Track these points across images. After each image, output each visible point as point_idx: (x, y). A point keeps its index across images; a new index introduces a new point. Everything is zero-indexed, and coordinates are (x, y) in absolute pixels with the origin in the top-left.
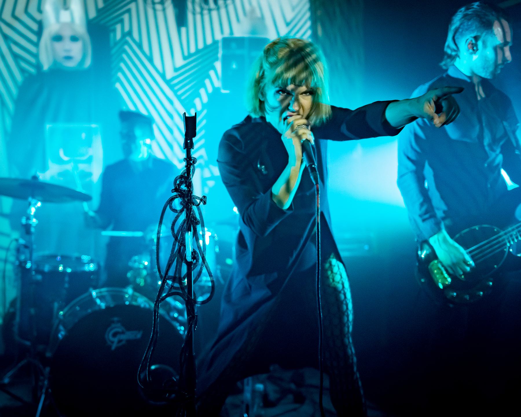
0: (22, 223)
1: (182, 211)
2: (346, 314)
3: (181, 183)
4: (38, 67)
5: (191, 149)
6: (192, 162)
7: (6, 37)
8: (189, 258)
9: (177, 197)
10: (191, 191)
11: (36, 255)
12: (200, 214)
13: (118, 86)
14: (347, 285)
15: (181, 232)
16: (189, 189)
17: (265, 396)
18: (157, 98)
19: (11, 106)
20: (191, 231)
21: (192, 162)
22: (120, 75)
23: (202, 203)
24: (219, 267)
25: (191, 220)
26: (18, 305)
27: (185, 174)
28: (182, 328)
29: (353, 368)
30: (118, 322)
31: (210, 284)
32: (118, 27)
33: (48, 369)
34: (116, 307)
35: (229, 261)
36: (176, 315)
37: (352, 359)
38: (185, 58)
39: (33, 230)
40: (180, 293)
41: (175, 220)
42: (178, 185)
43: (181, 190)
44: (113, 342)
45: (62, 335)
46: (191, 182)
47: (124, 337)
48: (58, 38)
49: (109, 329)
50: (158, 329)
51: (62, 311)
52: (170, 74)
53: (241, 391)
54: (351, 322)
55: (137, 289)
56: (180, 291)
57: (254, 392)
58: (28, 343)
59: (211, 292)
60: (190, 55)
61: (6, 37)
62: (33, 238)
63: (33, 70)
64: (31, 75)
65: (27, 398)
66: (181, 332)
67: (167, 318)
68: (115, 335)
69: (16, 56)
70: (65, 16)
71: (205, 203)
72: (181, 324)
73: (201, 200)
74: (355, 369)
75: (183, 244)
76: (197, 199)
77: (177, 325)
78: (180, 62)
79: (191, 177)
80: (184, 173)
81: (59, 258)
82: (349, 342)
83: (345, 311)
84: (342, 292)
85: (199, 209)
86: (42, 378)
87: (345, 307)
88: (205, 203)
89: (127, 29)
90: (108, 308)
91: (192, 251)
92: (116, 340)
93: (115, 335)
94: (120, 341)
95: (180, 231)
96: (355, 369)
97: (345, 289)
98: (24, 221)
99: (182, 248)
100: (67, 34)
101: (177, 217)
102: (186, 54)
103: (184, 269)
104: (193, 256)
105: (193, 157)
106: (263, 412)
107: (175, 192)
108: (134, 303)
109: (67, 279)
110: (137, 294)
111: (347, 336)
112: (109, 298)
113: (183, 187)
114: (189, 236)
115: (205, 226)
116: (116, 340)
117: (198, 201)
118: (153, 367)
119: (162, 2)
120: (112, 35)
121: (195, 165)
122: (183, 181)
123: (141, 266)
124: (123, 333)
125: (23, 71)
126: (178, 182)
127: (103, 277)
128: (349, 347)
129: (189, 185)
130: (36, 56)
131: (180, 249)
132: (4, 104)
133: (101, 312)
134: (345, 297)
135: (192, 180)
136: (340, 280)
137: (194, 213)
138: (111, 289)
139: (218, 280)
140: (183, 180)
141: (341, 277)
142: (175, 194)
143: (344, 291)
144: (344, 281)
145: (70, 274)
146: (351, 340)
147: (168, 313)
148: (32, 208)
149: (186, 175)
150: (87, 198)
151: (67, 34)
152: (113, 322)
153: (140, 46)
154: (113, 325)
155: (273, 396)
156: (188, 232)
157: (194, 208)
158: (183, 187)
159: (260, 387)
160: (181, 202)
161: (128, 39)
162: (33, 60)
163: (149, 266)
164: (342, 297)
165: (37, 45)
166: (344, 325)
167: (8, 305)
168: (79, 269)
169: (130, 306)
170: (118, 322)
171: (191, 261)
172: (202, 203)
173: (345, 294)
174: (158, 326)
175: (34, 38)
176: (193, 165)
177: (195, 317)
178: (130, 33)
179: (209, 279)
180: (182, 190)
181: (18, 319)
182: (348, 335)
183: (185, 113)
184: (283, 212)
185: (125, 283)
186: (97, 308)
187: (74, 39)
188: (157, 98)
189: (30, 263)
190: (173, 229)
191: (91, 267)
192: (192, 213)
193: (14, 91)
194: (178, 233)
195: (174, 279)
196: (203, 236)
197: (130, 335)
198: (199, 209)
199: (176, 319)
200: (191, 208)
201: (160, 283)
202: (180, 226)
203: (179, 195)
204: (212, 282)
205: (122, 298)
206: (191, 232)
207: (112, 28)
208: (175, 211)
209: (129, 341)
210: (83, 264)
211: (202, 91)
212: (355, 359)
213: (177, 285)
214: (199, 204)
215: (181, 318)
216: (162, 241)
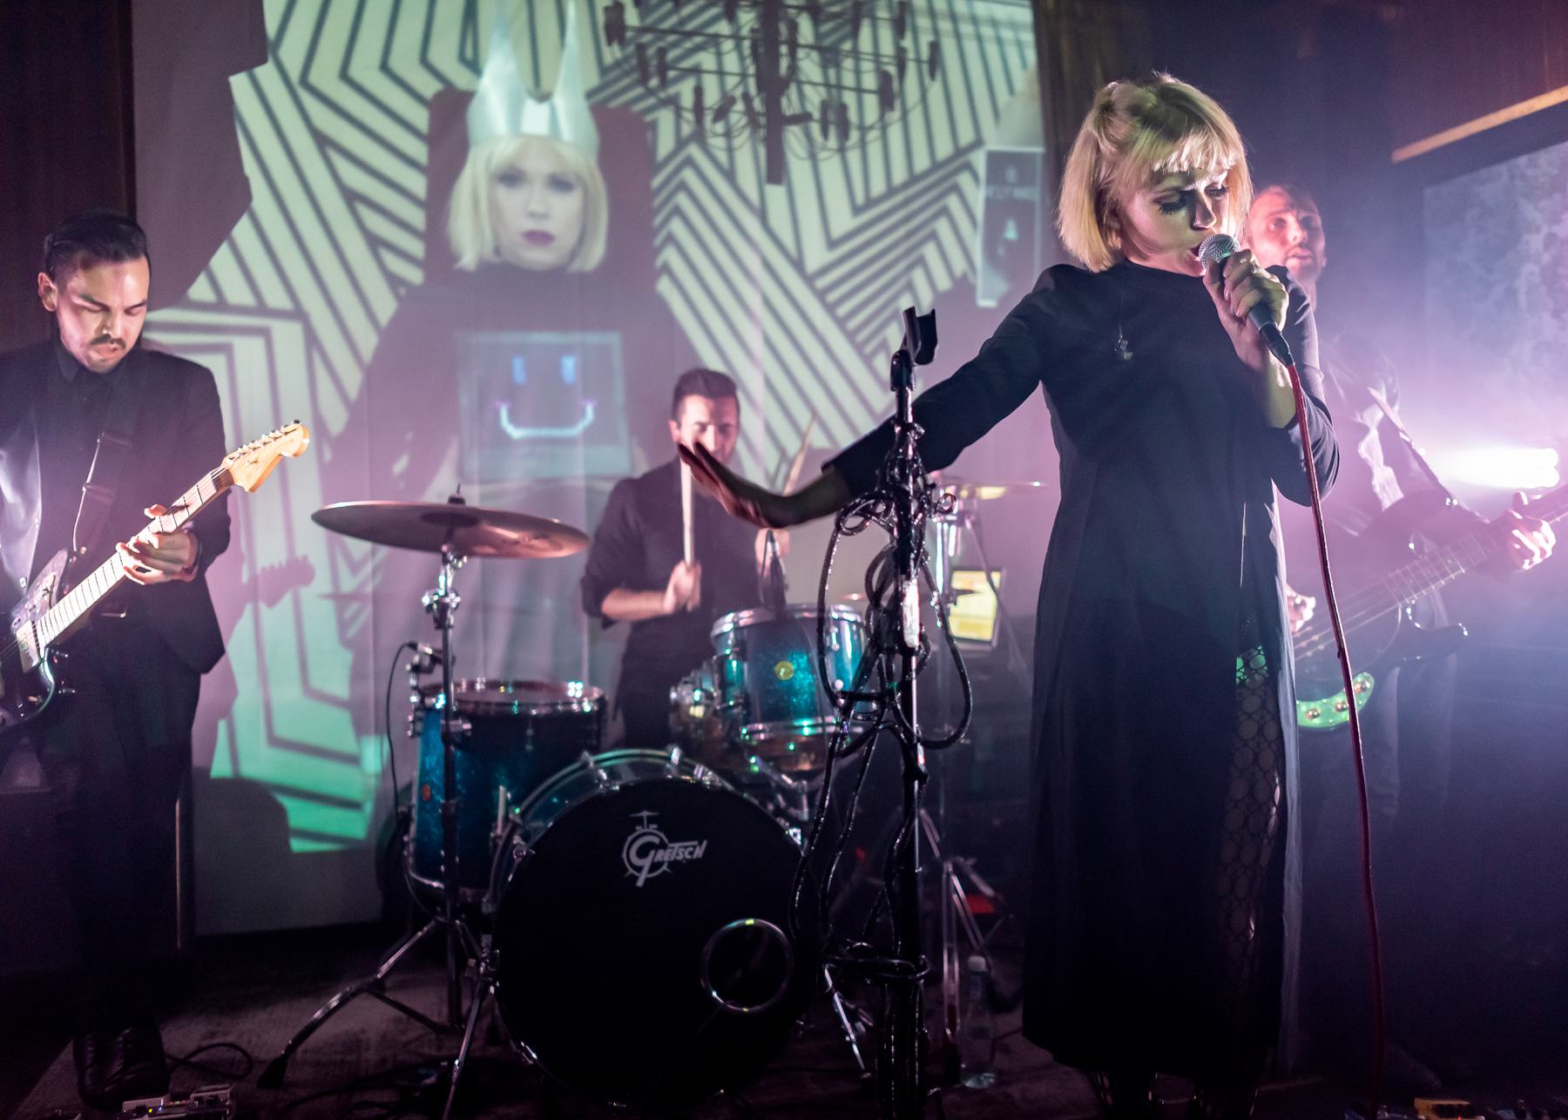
18: (973, 931)
22: (676, 226)
30: (651, 820)
32: (665, 118)
38: (857, 210)
39: (452, 619)
44: (639, 869)
48: (511, 177)
51: (519, 807)
52: (816, 256)
55: (692, 752)
57: (967, 974)
60: (870, 203)
68: (642, 853)
69: (352, 198)
70: (535, 118)
72: (795, 822)
78: (843, 222)
86: (472, 962)
92: (646, 863)
94: (655, 866)
100: (538, 166)
102: (860, 198)
106: (986, 1022)
116: (646, 863)
124: (663, 846)
125: (393, 281)
151: (538, 166)
152: (640, 821)
161: (694, 150)
169: (677, 782)
170: (651, 820)
187: (559, 183)
188: (973, 931)
193: (368, 342)
197: (680, 851)
207: (649, 118)
209: (673, 864)
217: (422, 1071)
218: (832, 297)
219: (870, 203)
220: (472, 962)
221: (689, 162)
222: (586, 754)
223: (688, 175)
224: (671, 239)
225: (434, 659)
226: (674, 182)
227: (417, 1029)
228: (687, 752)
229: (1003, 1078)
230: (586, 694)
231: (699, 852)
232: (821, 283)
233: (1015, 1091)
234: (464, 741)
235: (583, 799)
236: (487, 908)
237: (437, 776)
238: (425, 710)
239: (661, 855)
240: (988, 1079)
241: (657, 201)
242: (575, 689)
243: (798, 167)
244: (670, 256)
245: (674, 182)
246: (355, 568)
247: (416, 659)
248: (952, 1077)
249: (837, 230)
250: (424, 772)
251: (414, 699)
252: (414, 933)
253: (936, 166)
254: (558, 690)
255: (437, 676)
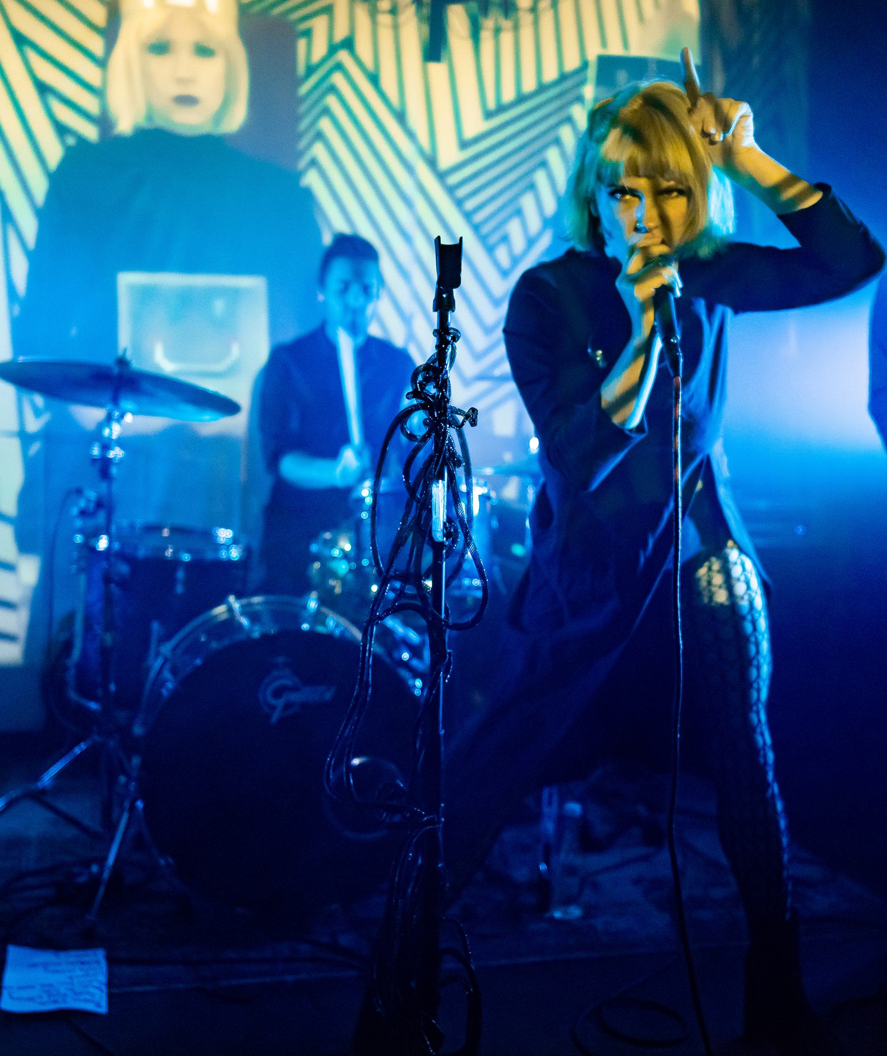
0: (92, 455)
1: (424, 439)
2: (755, 662)
3: (427, 380)
4: (104, 121)
5: (448, 311)
6: (450, 338)
7: (20, 40)
8: (439, 535)
9: (418, 409)
10: (446, 398)
11: (121, 520)
12: (464, 445)
13: (311, 179)
14: (759, 602)
15: (424, 481)
16: (443, 393)
17: (583, 825)
19: (29, 225)
20: (443, 479)
21: (450, 338)
22: (325, 125)
23: (467, 423)
24: (497, 559)
25: (445, 456)
26: (79, 626)
27: (436, 362)
28: (419, 683)
29: (765, 773)
31: (479, 594)
32: (319, 25)
33: (136, 761)
34: (282, 634)
35: (518, 550)
36: (406, 656)
37: (765, 756)
38: (489, 115)
39: (114, 471)
40: (417, 605)
41: (412, 456)
42: (421, 384)
43: (426, 395)
44: (273, 708)
45: (168, 690)
46: (448, 378)
47: (295, 697)
49: (266, 681)
50: (370, 679)
52: (449, 154)
53: (536, 817)
54: (764, 681)
55: (328, 600)
56: (418, 603)
57: (562, 819)
58: (94, 706)
59: (462, 572)
60: (501, 108)
61: (20, 40)
62: (115, 486)
63: (91, 132)
64: (82, 141)
65: (90, 819)
66: (417, 692)
67: (387, 660)
68: (277, 693)
69: (43, 89)
71: (474, 423)
72: (416, 674)
73: (467, 417)
74: (770, 776)
75: (426, 504)
76: (458, 414)
77: (404, 673)
78: (474, 125)
79: (447, 369)
80: (434, 362)
81: (166, 533)
82: (759, 721)
83: (754, 658)
84: (749, 618)
85: (461, 435)
87: (753, 649)
88: (474, 423)
89: (340, 34)
90: (265, 637)
91: (445, 521)
92: (280, 703)
93: (277, 693)
94: (287, 706)
95: (422, 479)
96: (770, 776)
97: (754, 613)
98: (96, 451)
99: (424, 513)
101: (417, 450)
103: (428, 558)
104: (446, 530)
105: (452, 328)
106: (578, 861)
107: (413, 397)
108: (320, 629)
109: (180, 574)
110: (325, 610)
111: (755, 708)
112: (266, 618)
113: (432, 390)
114: (439, 491)
115: (413, 370)
116: (280, 703)
117: (460, 418)
118: (356, 762)
119: (394, 11)
120: (302, 44)
121: (457, 344)
122: (432, 376)
123: (336, 553)
124: (295, 689)
125: (62, 130)
126: (420, 378)
127: (257, 575)
128: (758, 730)
129: (443, 385)
130: (98, 92)
131: (418, 518)
132: (8, 217)
133: (251, 644)
134: (755, 629)
135: (449, 375)
136: (745, 593)
137: (451, 444)
138: (272, 598)
139: (494, 584)
140: (431, 373)
141: (749, 587)
142: (414, 402)
143: (753, 616)
144: (753, 594)
145: (189, 566)
146: (763, 717)
147: (390, 654)
148: (315, 62)
149: (437, 364)
150: (228, 407)
153: (374, 79)
154: (275, 673)
155: (601, 829)
156: (438, 482)
157: (452, 432)
158: (432, 390)
159: (574, 808)
160: (426, 420)
161: (343, 56)
162: (91, 104)
163: (353, 554)
164: (748, 627)
165: (102, 63)
166: (750, 685)
167: (56, 627)
168: (209, 556)
169: (311, 633)
171: (442, 540)
172: (467, 423)
173: (754, 623)
174: (370, 672)
175: (96, 45)
176: (452, 345)
177: (448, 656)
178: (349, 44)
179: (477, 582)
180: (428, 395)
181: (76, 653)
182: (758, 708)
183: (439, 238)
184: (620, 436)
185: (303, 587)
186: (240, 637)
187: (203, 51)
189: (105, 539)
190: (406, 472)
191: (235, 554)
192: (447, 442)
193: (40, 187)
194: (417, 483)
195: (405, 578)
196: (469, 494)
198: (461, 435)
199: (406, 665)
200: (445, 432)
201: (374, 588)
202: (422, 469)
203: (421, 404)
204: (484, 588)
205: (297, 619)
206: (443, 482)
207: (303, 26)
208: (411, 437)
209: (304, 706)
210: (217, 547)
211: (528, 202)
212: (771, 756)
213: (410, 590)
214: (463, 424)
215: (415, 663)
216: (381, 501)
217: (76, 870)
218: (462, 192)
219: (501, 108)
220: (122, 779)
221: (339, 67)
222: (232, 599)
223: (338, 79)
224: (320, 136)
225: (99, 505)
226: (325, 85)
227: (71, 832)
228: (322, 601)
229: (590, 912)
230: (235, 541)
231: (328, 696)
232: (453, 180)
233: (598, 923)
234: (123, 584)
235: (226, 642)
236: (138, 730)
237: (98, 607)
238: (89, 549)
239: (295, 697)
240: (575, 912)
241: (303, 108)
242: (224, 534)
243: (486, 36)
244: (318, 151)
245: (325, 85)
246: (37, 413)
247: (82, 504)
248: (545, 905)
249: (470, 132)
250: (88, 607)
251: (79, 539)
252: (71, 748)
253: (563, 77)
254: (208, 535)
255: (101, 518)
